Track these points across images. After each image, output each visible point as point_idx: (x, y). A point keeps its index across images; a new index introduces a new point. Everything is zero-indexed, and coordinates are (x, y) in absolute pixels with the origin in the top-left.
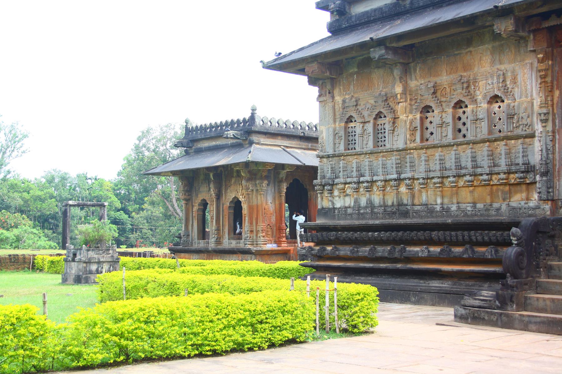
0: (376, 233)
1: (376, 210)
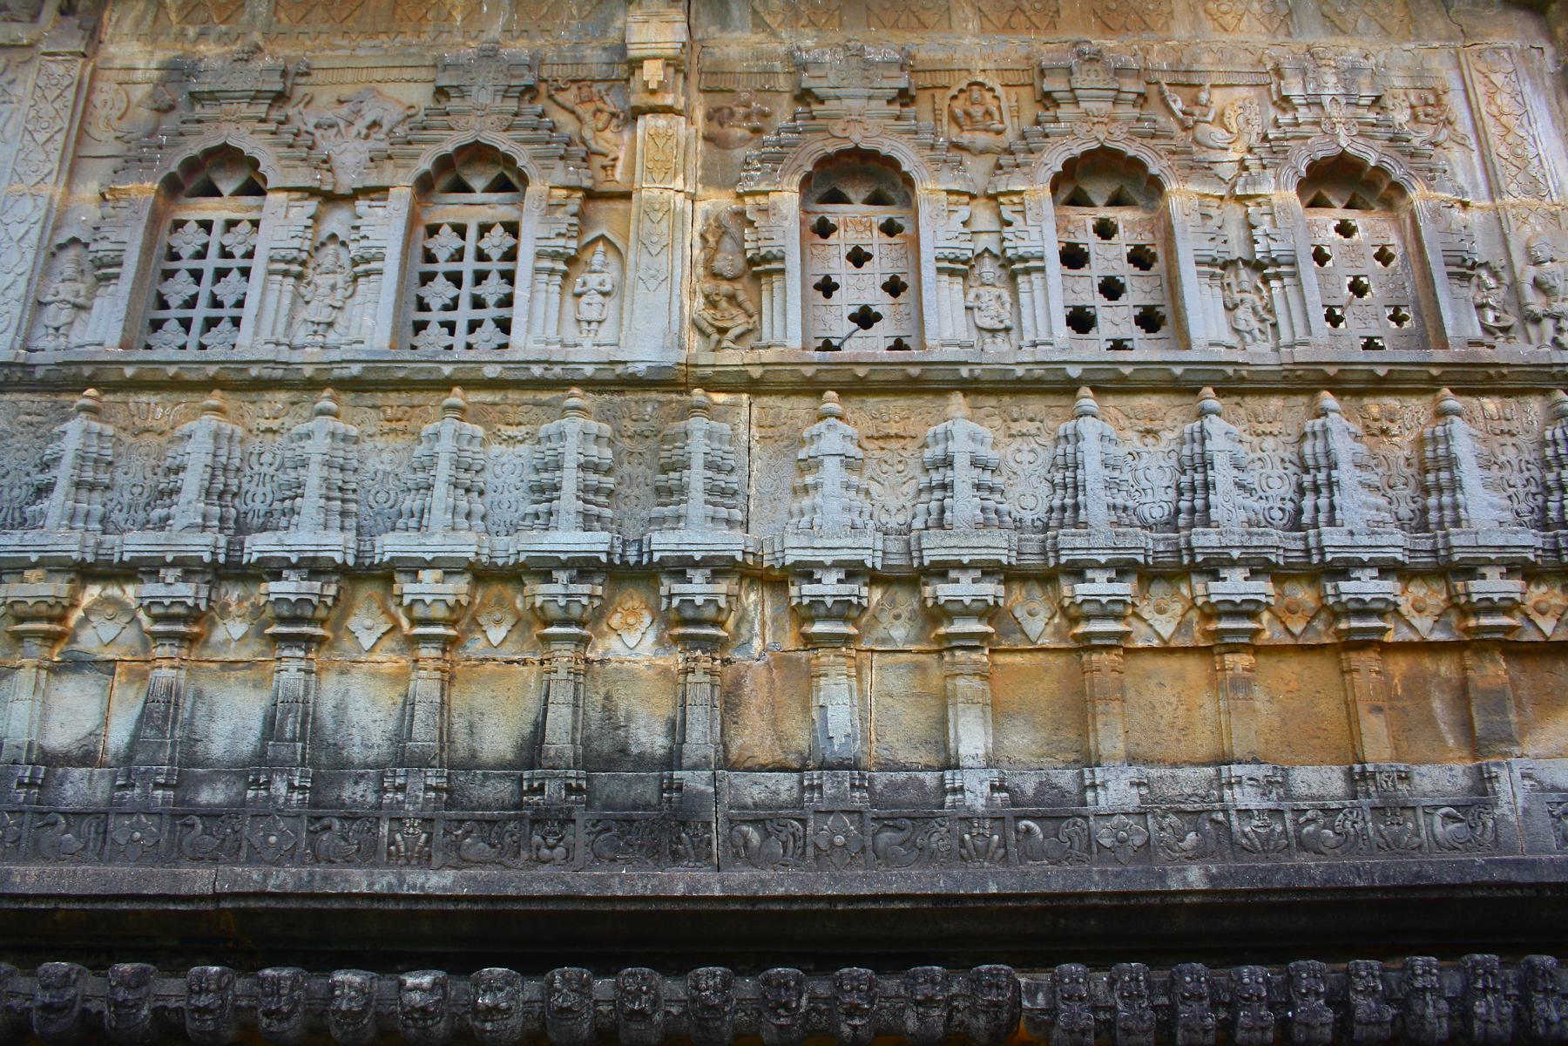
0: (216, 968)
1: (357, 793)
